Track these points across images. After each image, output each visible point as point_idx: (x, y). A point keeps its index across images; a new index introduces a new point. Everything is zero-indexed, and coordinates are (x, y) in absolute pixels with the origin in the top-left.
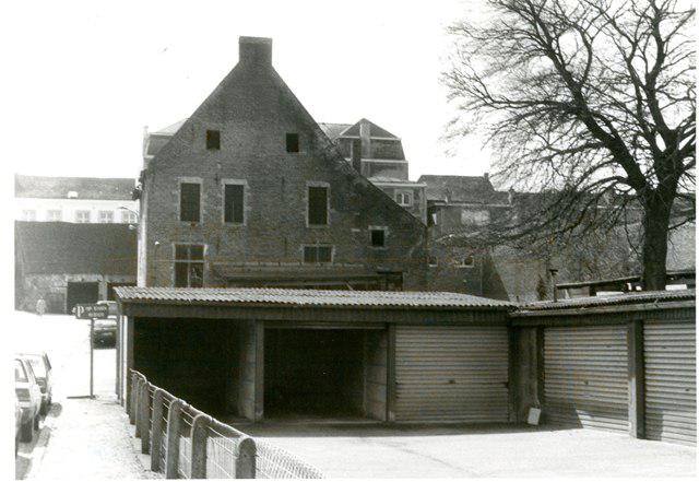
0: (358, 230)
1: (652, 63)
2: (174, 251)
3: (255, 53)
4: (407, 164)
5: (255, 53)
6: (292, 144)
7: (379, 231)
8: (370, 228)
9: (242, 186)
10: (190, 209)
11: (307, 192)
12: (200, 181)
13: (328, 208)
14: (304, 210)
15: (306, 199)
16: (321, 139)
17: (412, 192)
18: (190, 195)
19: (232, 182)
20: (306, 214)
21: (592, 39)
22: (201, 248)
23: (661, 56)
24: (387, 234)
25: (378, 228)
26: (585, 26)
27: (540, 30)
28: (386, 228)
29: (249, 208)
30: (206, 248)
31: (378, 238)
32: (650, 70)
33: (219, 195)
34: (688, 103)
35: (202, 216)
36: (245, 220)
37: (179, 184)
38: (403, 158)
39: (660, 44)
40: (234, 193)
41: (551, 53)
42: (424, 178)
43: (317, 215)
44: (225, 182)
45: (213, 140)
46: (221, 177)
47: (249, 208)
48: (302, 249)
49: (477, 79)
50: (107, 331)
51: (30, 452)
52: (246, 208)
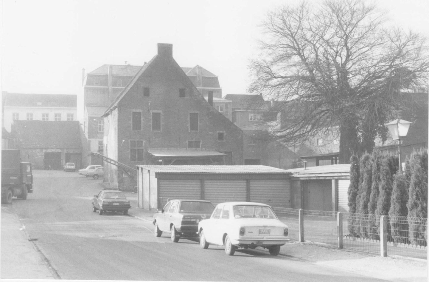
0: (212, 133)
1: (344, 60)
2: (130, 143)
3: (165, 51)
4: (220, 90)
5: (165, 51)
6: (182, 93)
7: (221, 133)
8: (218, 132)
9: (160, 113)
10: (137, 123)
11: (189, 115)
12: (141, 111)
13: (199, 123)
14: (188, 124)
15: (189, 119)
16: (195, 91)
17: (224, 105)
18: (137, 118)
19: (156, 111)
20: (189, 125)
21: (318, 48)
22: (142, 142)
23: (348, 56)
24: (225, 134)
25: (221, 132)
26: (314, 43)
27: (295, 45)
28: (224, 132)
29: (163, 123)
30: (144, 142)
31: (221, 136)
32: (343, 63)
33: (150, 118)
34: (321, 46)
35: (142, 127)
36: (161, 128)
37: (132, 113)
38: (219, 86)
39: (348, 50)
40: (156, 117)
41: (299, 54)
42: (228, 97)
43: (194, 126)
44: (152, 111)
45: (146, 92)
46: (150, 109)
47: (163, 123)
48: (187, 142)
49: (268, 67)
50: (116, 202)
51: (18, 124)
52: (162, 123)
